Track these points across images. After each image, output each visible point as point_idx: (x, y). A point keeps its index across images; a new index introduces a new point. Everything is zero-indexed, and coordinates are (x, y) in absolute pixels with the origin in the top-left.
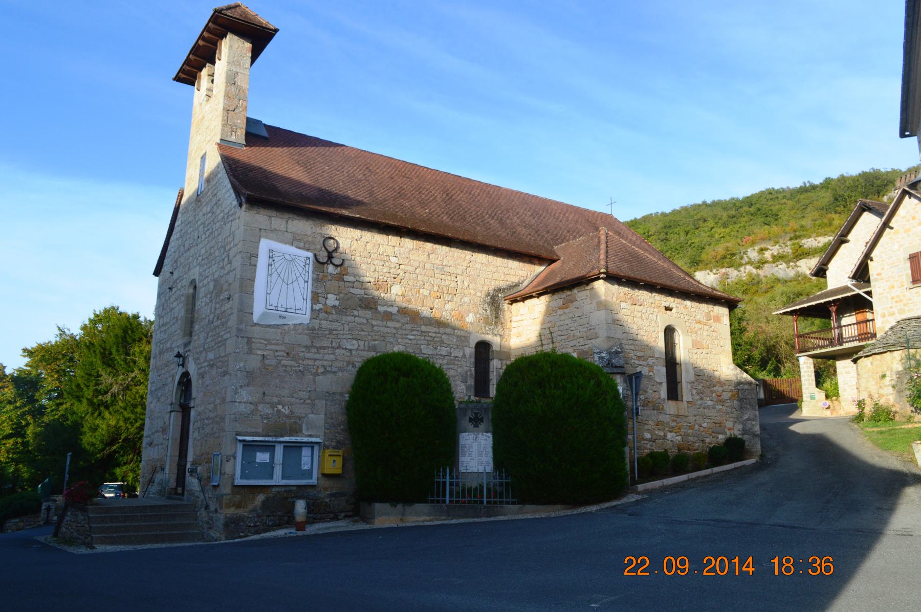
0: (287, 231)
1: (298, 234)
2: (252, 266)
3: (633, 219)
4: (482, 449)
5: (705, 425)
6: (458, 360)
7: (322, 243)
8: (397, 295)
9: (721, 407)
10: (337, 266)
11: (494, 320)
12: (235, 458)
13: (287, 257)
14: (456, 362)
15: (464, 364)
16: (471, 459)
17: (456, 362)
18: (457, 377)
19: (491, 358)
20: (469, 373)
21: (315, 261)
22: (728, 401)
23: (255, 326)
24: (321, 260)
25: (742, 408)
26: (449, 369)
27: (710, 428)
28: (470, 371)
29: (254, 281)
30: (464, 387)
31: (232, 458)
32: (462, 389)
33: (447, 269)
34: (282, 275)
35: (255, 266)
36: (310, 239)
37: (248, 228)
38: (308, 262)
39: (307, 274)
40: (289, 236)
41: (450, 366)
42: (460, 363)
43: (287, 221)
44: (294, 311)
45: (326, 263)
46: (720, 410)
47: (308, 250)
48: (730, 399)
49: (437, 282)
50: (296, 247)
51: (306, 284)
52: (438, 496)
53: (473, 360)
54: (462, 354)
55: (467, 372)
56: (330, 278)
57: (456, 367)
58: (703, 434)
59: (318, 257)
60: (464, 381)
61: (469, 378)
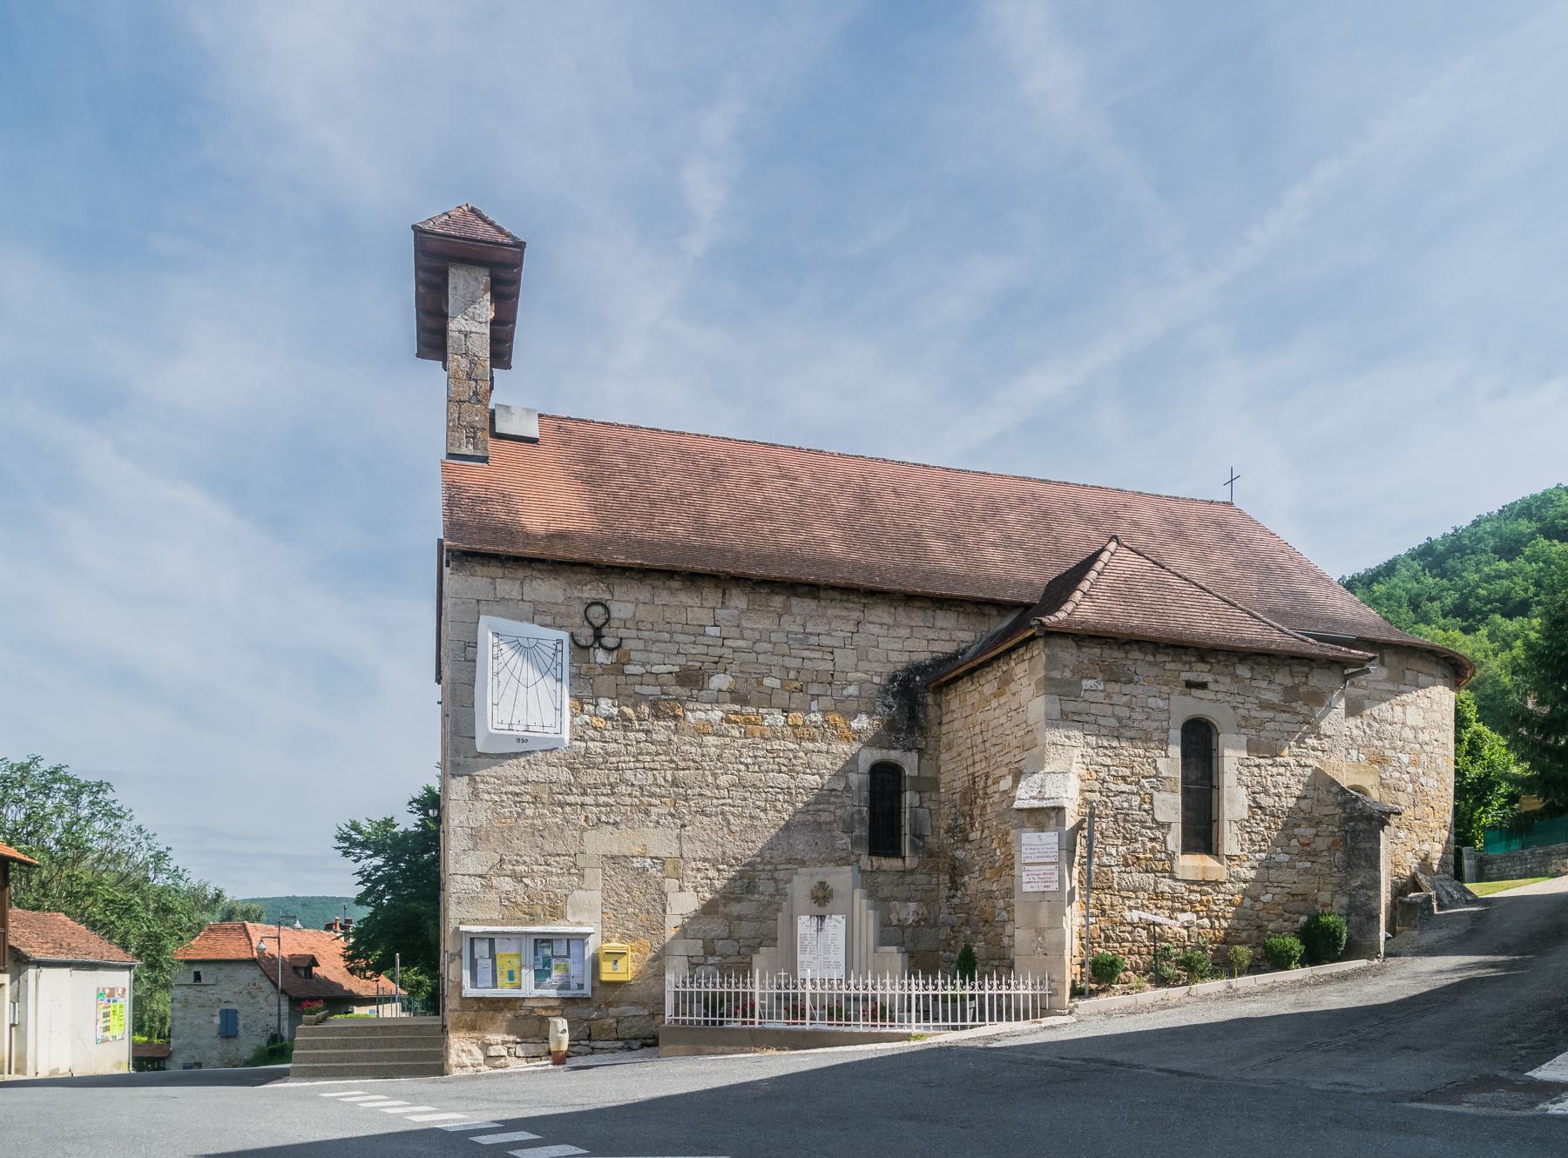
0: (522, 600)
1: (541, 603)
2: (469, 661)
3: (1539, 491)
4: (829, 942)
5: (1267, 898)
6: (836, 796)
7: (582, 612)
8: (720, 690)
9: (1308, 865)
10: (609, 650)
11: (906, 722)
12: (461, 958)
13: (523, 642)
14: (832, 799)
15: (847, 801)
16: (814, 958)
17: (832, 799)
18: (835, 825)
19: (903, 789)
20: (856, 817)
21: (573, 645)
22: (1325, 853)
23: (479, 757)
24: (583, 642)
25: (1350, 867)
26: (820, 810)
27: (1279, 904)
28: (860, 812)
29: (473, 687)
30: (848, 840)
31: (457, 958)
32: (845, 844)
33: (813, 640)
34: (516, 673)
35: (474, 661)
36: (563, 609)
37: (459, 601)
38: (559, 647)
39: (559, 668)
40: (527, 608)
41: (821, 807)
42: (840, 800)
43: (522, 583)
44: (541, 729)
45: (591, 646)
46: (1306, 870)
47: (560, 627)
48: (1329, 849)
49: (796, 663)
50: (539, 625)
51: (559, 684)
52: (954, 1020)
53: (865, 794)
54: (842, 785)
55: (852, 815)
56: (600, 670)
57: (832, 808)
58: (1261, 914)
59: (576, 638)
60: (848, 829)
61: (856, 825)
